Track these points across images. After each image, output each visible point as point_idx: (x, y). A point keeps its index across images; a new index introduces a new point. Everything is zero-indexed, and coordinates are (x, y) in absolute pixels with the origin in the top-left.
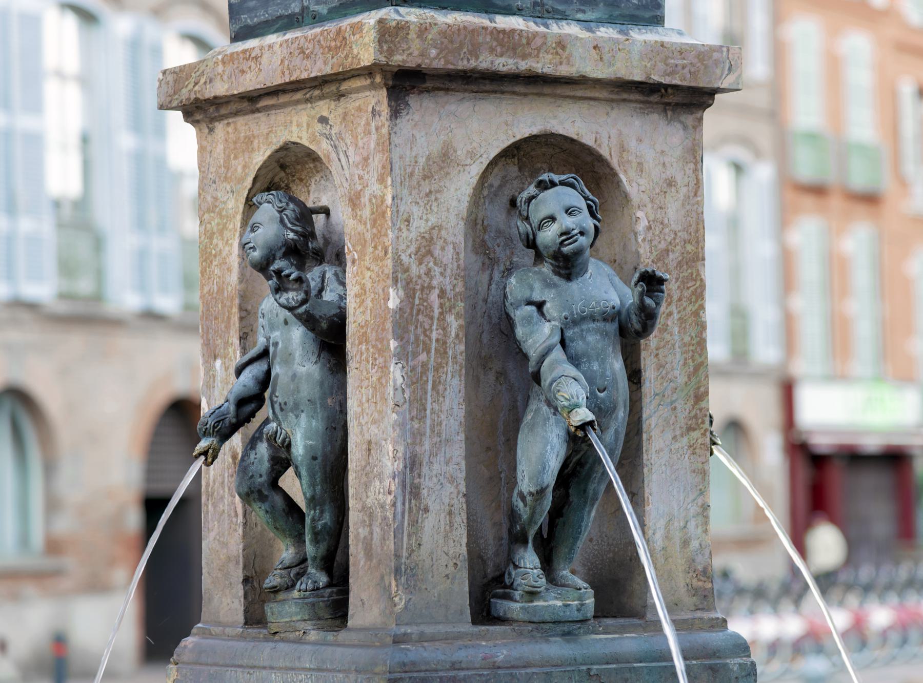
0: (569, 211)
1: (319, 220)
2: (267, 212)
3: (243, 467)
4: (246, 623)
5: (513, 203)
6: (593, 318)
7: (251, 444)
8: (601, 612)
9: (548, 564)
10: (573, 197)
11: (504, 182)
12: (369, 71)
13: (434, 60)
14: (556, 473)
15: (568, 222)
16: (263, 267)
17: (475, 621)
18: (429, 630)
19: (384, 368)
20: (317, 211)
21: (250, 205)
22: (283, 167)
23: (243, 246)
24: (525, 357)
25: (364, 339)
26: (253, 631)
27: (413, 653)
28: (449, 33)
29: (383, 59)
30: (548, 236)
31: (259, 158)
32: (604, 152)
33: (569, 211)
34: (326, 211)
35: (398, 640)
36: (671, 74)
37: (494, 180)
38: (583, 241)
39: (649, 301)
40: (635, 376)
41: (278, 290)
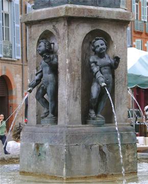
0: (102, 45)
1: (52, 45)
2: (42, 44)
3: (37, 94)
4: (37, 124)
5: (91, 43)
6: (106, 66)
7: (38, 90)
8: (107, 122)
9: (96, 113)
10: (102, 42)
11: (89, 38)
12: (63, 17)
13: (76, 15)
14: (80, 63)
15: (101, 47)
16: (41, 54)
17: (82, 124)
18: (74, 125)
19: (66, 75)
20: (52, 43)
21: (39, 42)
22: (45, 35)
23: (37, 50)
24: (93, 72)
25: (62, 69)
26: (38, 125)
27: (133, 176)
28: (79, 9)
29: (66, 15)
30: (98, 49)
31: (40, 34)
32: (118, 68)
33: (102, 45)
34: (54, 44)
35: (68, 127)
36: (122, 17)
37: (87, 38)
38: (104, 50)
39: (117, 62)
40: (114, 77)
41: (44, 59)
